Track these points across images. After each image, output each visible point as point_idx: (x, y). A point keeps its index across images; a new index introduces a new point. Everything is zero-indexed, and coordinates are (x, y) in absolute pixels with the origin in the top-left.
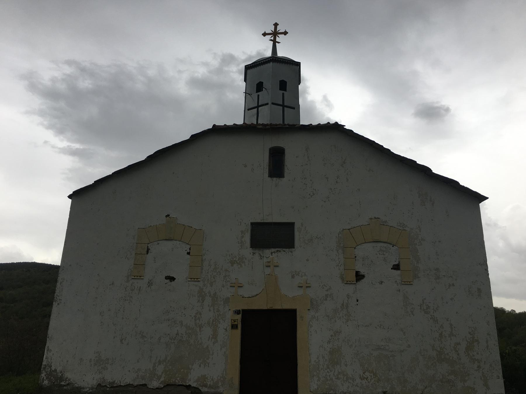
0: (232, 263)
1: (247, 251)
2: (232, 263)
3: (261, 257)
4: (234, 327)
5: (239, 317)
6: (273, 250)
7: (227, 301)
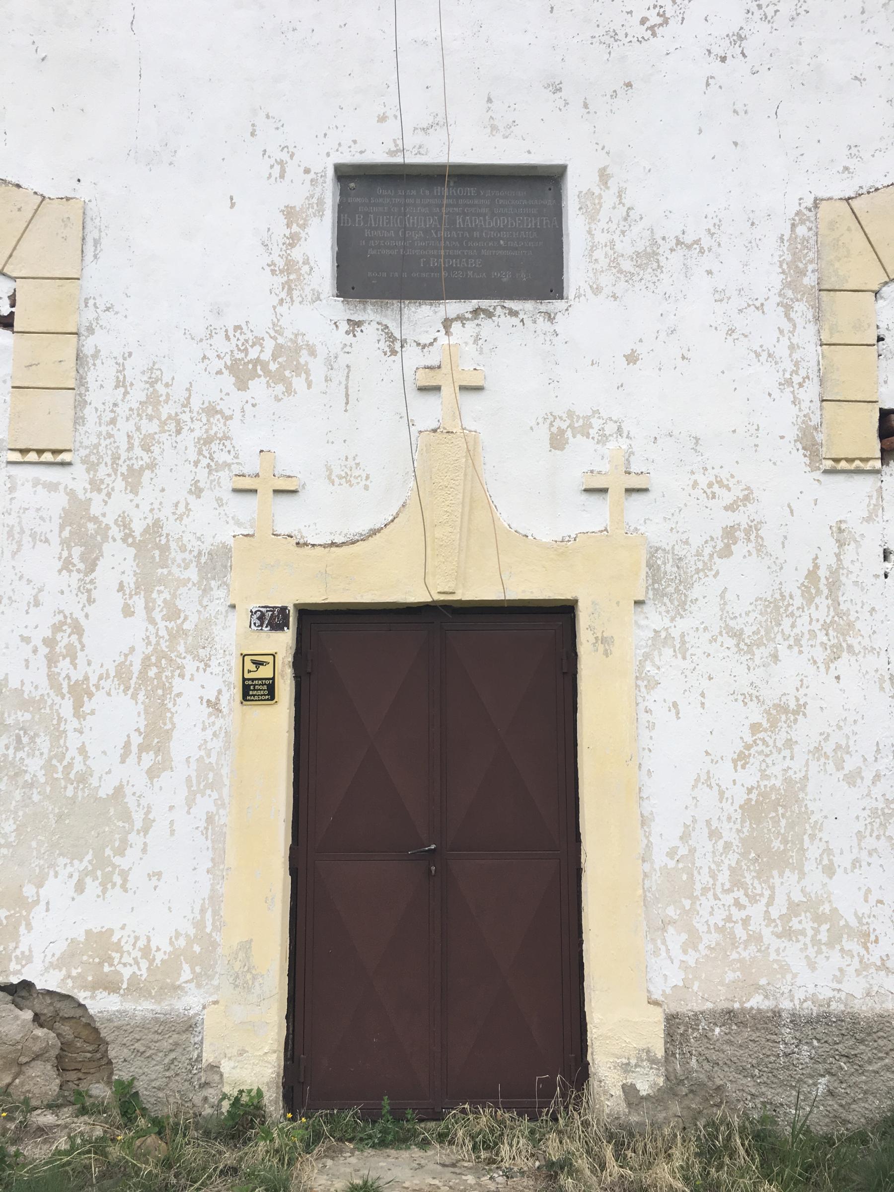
0: (242, 372)
1: (320, 314)
2: (242, 372)
3: (394, 344)
4: (257, 690)
5: (282, 644)
6: (454, 307)
7: (216, 563)
